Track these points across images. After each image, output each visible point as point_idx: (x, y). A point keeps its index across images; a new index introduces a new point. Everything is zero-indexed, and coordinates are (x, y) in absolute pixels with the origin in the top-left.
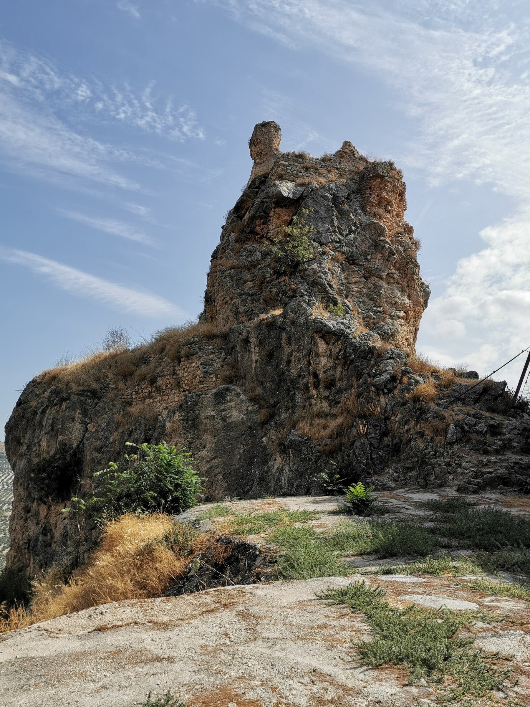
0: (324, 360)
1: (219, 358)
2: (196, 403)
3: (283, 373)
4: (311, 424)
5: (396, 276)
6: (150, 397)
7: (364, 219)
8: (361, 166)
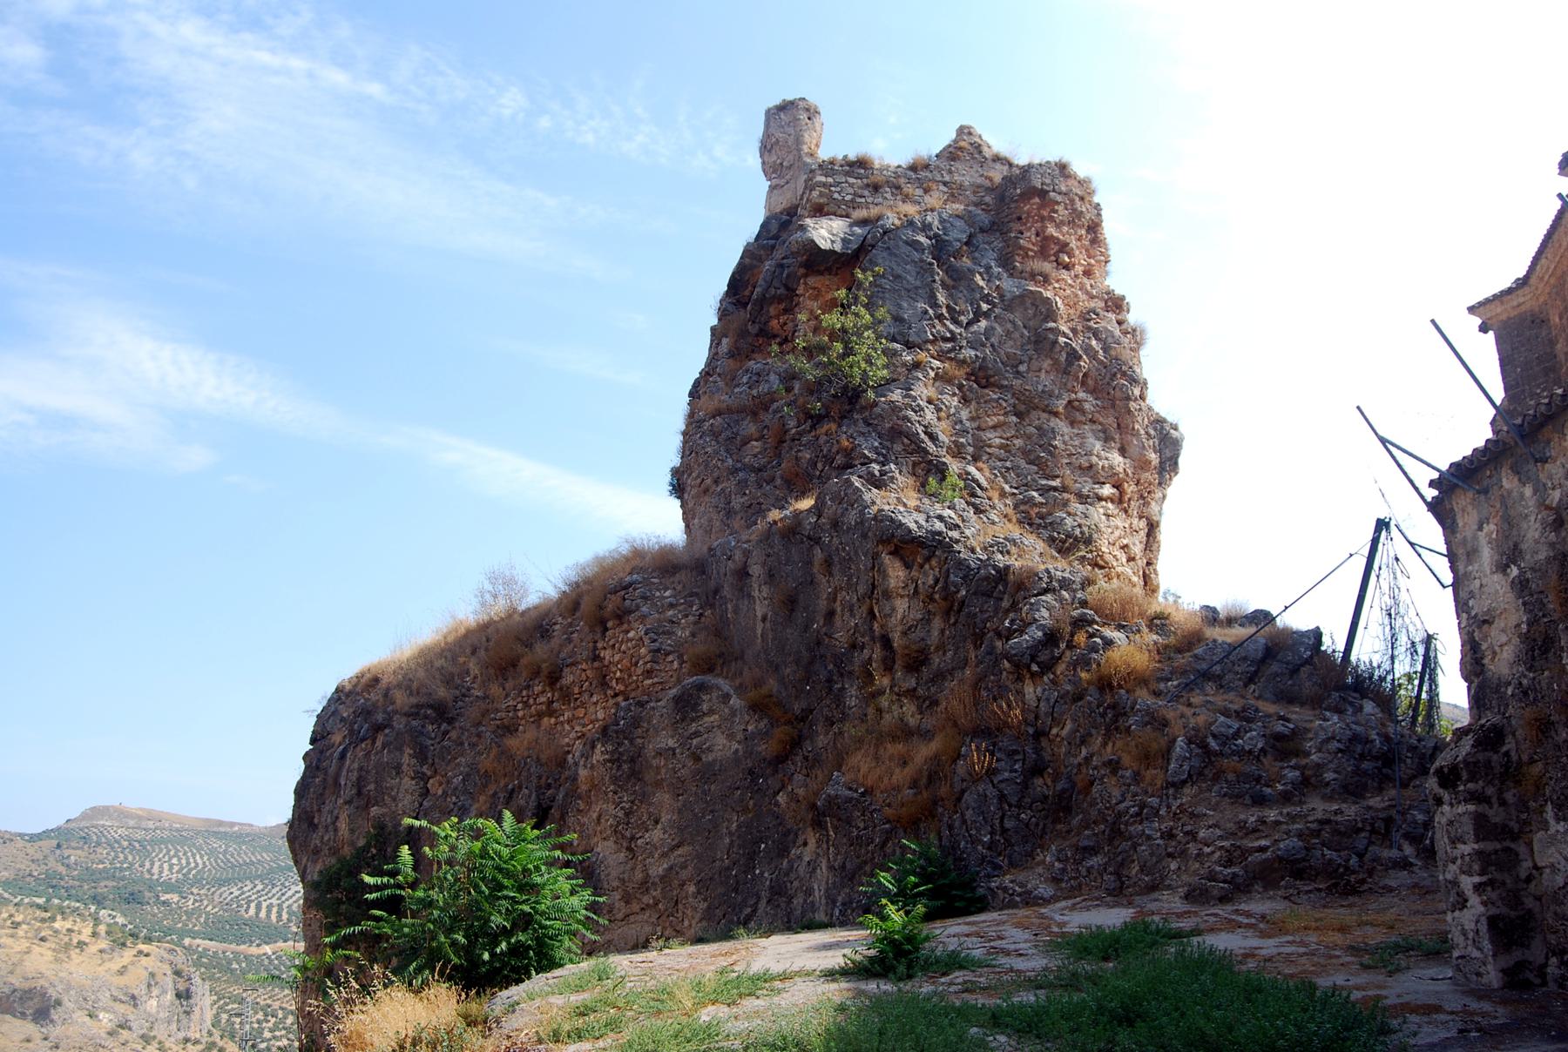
0: (901, 605)
2: (636, 722)
3: (819, 643)
4: (877, 758)
5: (1087, 406)
6: (551, 713)
7: (1009, 285)
8: (997, 174)
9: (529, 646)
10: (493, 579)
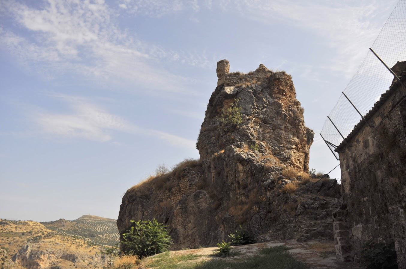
0: (242, 174)
1: (197, 176)
2: (186, 200)
5: (289, 127)
6: (169, 198)
7: (271, 100)
8: (269, 75)
9: (165, 183)
10: (159, 167)
